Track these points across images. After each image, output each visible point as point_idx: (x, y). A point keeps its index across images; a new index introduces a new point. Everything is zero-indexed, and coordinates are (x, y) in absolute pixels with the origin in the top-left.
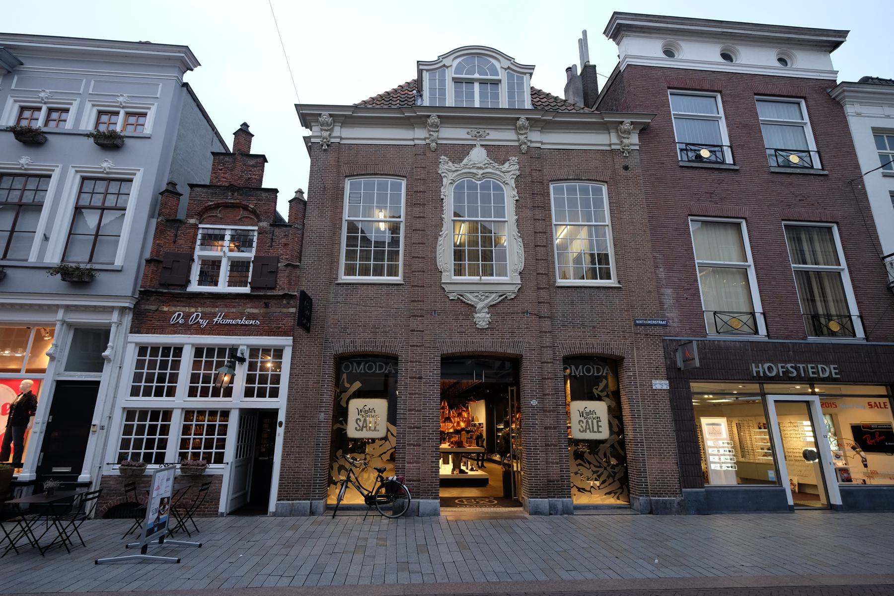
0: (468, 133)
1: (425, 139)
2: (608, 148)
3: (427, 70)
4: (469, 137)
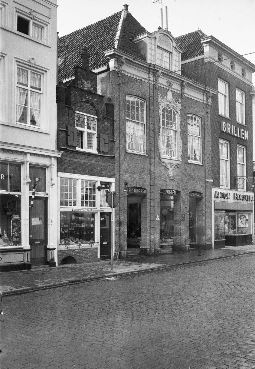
0: (167, 82)
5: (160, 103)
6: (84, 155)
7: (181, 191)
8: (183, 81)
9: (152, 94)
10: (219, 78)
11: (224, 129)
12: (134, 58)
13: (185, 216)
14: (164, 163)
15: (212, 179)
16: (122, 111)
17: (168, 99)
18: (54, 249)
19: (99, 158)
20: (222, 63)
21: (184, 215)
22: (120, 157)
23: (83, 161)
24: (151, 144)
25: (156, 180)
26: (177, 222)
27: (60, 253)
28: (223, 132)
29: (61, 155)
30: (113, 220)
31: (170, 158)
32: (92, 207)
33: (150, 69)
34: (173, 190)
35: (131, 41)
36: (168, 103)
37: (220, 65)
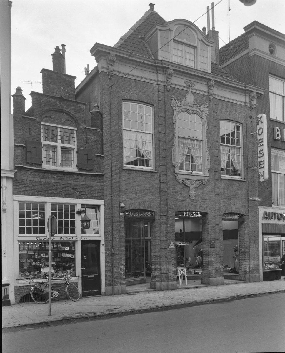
0: (185, 83)
1: (164, 82)
2: (244, 104)
3: (160, 30)
4: (185, 85)
5: (174, 108)
6: (55, 174)
7: (209, 212)
8: (210, 80)
9: (162, 97)
10: (270, 75)
11: (278, 135)
12: (222, 78)
13: (215, 242)
14: (181, 180)
15: (259, 197)
16: (115, 120)
17: (187, 103)
18: (8, 285)
19: (79, 177)
20: (277, 56)
21: (213, 241)
22: (113, 175)
23: (53, 181)
24: (161, 158)
25: (169, 201)
26: (206, 250)
27: (18, 289)
28: (276, 140)
29: (14, 175)
30: (103, 249)
31: (191, 173)
32: (39, 235)
33: (157, 66)
34: (195, 211)
35: (144, 40)
36: (188, 107)
37: (272, 58)
